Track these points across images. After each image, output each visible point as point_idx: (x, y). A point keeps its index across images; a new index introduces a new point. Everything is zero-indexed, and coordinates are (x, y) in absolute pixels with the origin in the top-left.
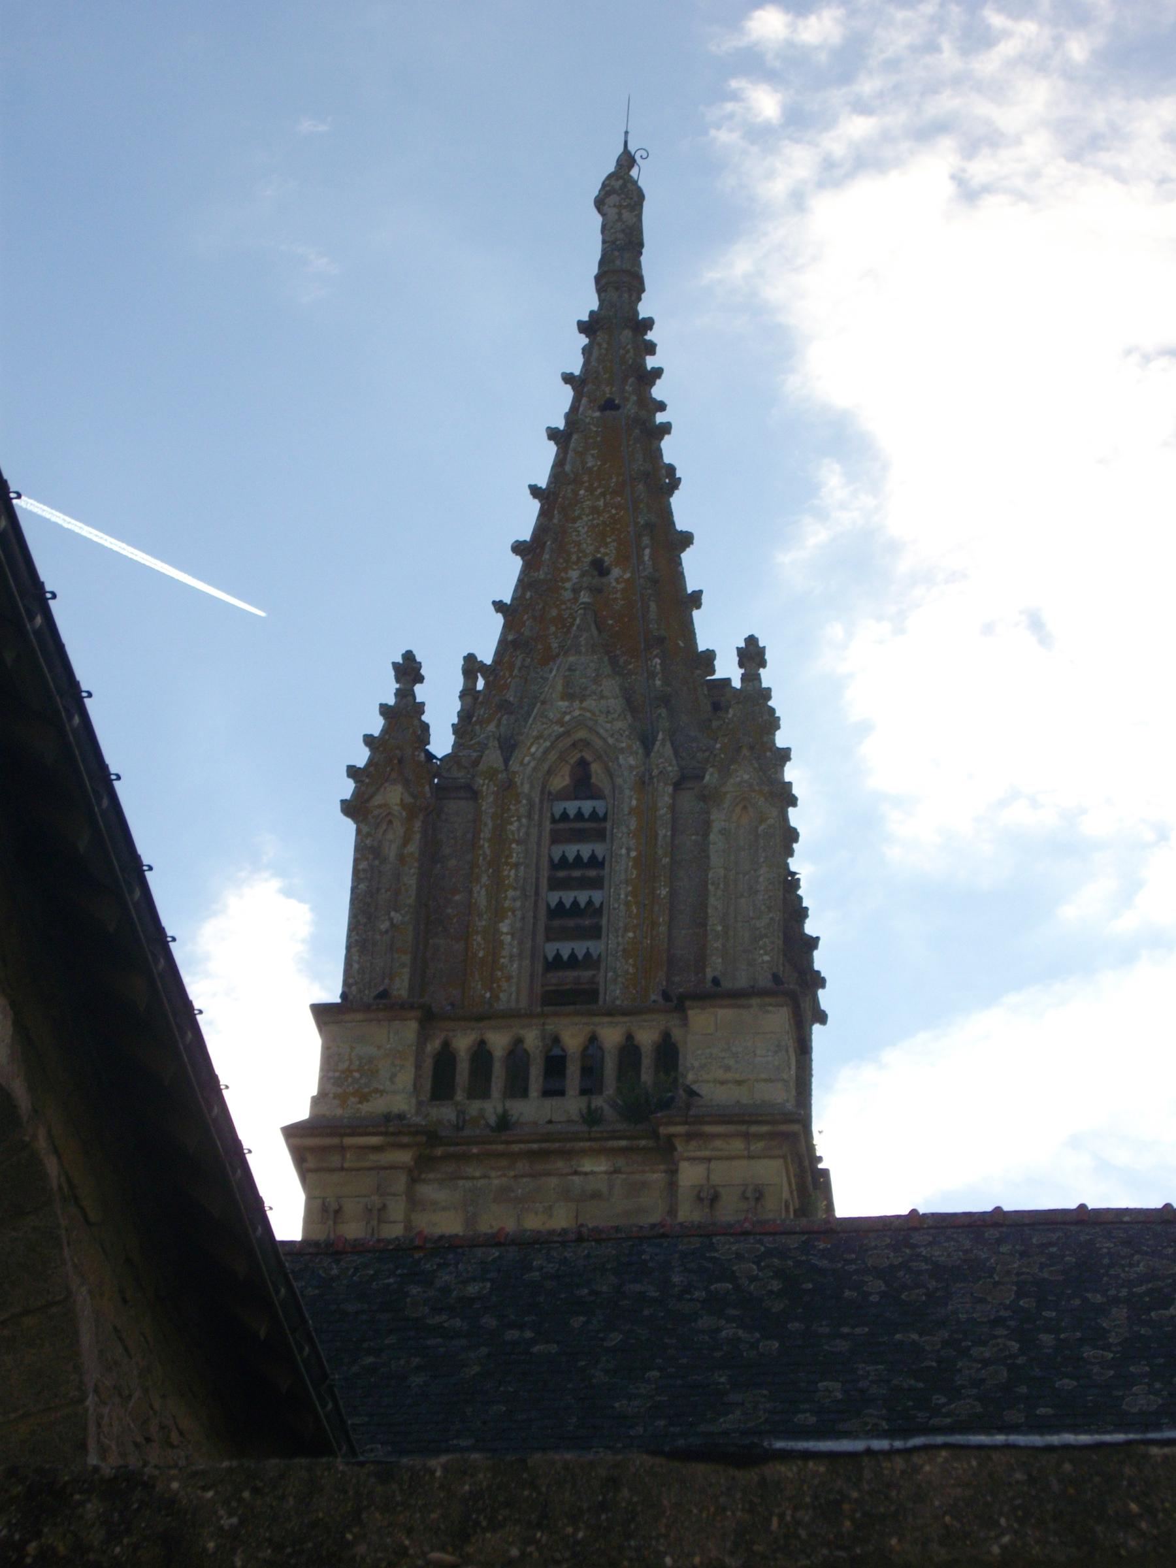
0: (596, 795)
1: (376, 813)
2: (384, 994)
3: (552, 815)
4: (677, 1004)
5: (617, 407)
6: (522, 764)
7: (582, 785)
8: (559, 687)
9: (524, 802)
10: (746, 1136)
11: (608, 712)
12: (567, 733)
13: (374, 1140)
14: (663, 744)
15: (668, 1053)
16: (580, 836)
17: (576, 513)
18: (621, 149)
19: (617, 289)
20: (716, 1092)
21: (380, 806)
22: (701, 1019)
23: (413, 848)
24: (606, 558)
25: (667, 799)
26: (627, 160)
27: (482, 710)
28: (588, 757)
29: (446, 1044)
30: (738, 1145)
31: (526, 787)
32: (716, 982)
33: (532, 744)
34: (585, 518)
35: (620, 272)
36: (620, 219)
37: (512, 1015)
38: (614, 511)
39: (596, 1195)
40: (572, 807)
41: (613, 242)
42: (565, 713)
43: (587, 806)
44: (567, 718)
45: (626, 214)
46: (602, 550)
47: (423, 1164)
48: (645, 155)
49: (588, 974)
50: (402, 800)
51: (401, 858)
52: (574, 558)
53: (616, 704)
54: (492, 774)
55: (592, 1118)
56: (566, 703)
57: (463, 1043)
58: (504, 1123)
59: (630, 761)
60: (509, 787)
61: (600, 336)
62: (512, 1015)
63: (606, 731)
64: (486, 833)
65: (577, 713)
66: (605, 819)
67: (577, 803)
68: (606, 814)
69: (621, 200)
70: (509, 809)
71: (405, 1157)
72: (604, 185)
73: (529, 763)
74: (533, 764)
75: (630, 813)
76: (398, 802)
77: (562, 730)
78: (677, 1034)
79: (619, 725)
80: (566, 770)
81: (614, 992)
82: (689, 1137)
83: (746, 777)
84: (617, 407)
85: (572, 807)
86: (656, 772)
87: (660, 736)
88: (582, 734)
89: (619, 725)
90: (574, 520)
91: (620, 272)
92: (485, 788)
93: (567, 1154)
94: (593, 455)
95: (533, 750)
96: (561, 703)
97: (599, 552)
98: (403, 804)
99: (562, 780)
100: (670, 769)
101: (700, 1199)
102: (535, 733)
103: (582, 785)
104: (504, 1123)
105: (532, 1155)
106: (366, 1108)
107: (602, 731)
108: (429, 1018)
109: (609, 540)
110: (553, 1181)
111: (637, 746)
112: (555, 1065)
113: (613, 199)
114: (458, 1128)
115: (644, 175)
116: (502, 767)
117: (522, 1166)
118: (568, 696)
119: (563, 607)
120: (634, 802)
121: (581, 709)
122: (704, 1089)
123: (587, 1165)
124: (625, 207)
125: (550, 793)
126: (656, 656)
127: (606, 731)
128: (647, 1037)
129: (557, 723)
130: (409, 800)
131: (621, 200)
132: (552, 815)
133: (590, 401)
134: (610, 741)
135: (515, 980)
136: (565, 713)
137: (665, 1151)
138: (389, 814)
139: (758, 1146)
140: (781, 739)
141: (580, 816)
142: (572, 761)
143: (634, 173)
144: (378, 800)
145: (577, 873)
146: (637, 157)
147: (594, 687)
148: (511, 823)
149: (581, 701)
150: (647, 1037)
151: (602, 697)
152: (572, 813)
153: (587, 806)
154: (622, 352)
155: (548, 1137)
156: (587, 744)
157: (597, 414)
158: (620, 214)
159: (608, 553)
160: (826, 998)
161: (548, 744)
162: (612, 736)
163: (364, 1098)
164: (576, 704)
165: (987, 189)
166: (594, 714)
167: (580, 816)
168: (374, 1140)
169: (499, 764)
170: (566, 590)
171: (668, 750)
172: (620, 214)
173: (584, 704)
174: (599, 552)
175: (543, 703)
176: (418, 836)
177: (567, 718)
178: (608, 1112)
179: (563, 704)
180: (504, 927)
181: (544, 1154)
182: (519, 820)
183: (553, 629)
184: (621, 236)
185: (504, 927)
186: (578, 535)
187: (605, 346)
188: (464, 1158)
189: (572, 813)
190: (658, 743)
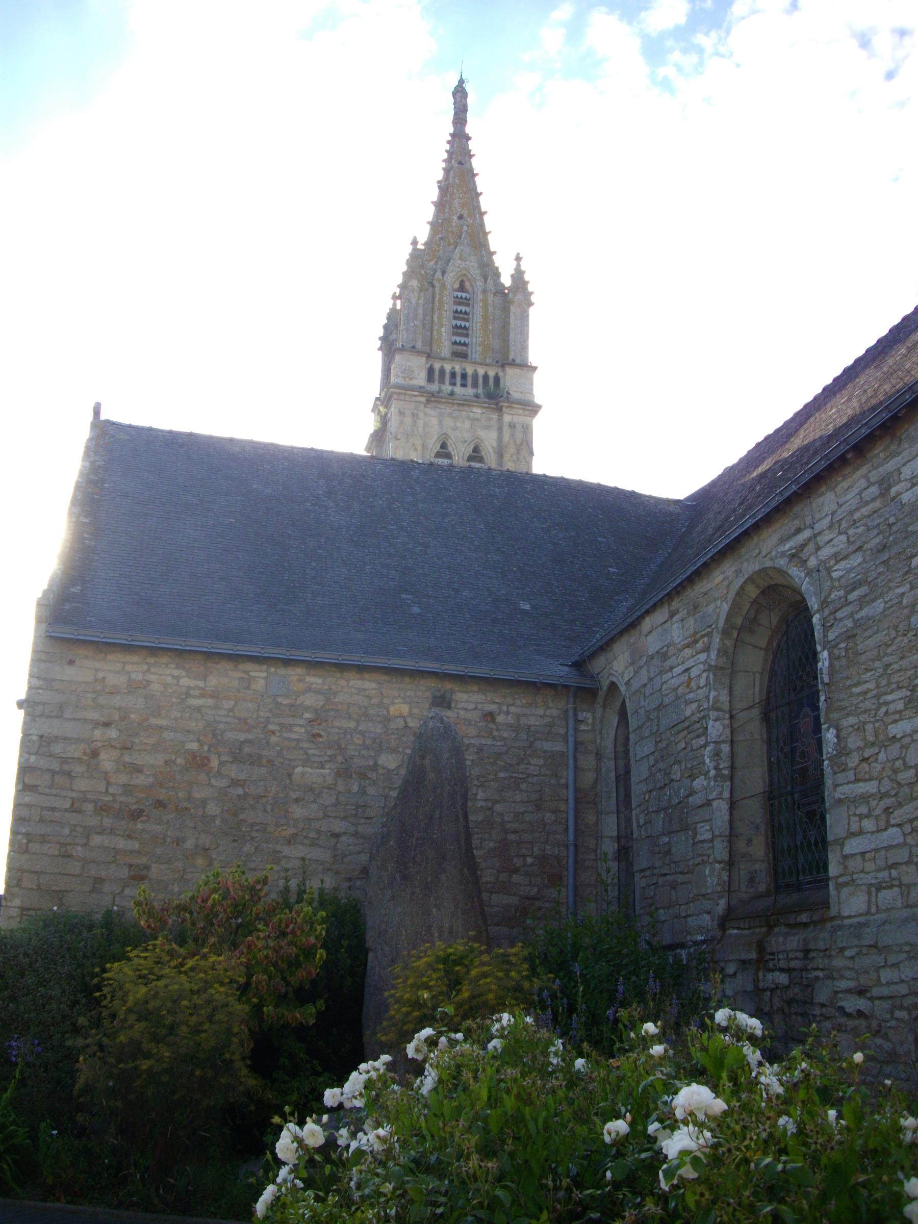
0: (467, 292)
2: (414, 347)
4: (503, 366)
7: (462, 288)
10: (524, 409)
13: (416, 393)
15: (497, 379)
16: (460, 304)
20: (515, 395)
22: (510, 371)
23: (421, 301)
26: (461, 82)
28: (465, 279)
29: (431, 366)
30: (521, 412)
32: (513, 360)
35: (460, 117)
37: (443, 359)
39: (477, 419)
43: (464, 295)
47: (428, 401)
49: (465, 348)
51: (418, 304)
53: (476, 265)
54: (439, 280)
55: (477, 396)
57: (437, 366)
58: (452, 394)
59: (480, 283)
60: (443, 286)
61: (457, 139)
62: (443, 359)
64: (437, 299)
69: (460, 93)
71: (423, 399)
78: (501, 374)
80: (458, 283)
81: (477, 357)
82: (507, 407)
85: (459, 294)
88: (464, 272)
91: (460, 117)
93: (469, 406)
99: (457, 286)
101: (510, 426)
103: (462, 288)
104: (452, 394)
105: (459, 405)
106: (411, 382)
108: (429, 356)
110: (464, 413)
112: (453, 375)
114: (438, 392)
115: (468, 87)
117: (455, 407)
118: (461, 259)
122: (511, 393)
123: (475, 410)
128: (491, 374)
131: (460, 93)
135: (446, 349)
137: (499, 410)
139: (527, 413)
141: (461, 297)
144: (410, 284)
145: (461, 316)
150: (491, 374)
153: (464, 295)
155: (466, 400)
159: (465, 213)
160: (379, 343)
163: (411, 379)
167: (461, 297)
168: (416, 393)
169: (441, 277)
171: (492, 282)
178: (482, 395)
179: (459, 262)
180: (443, 330)
181: (463, 405)
185: (443, 330)
188: (439, 402)
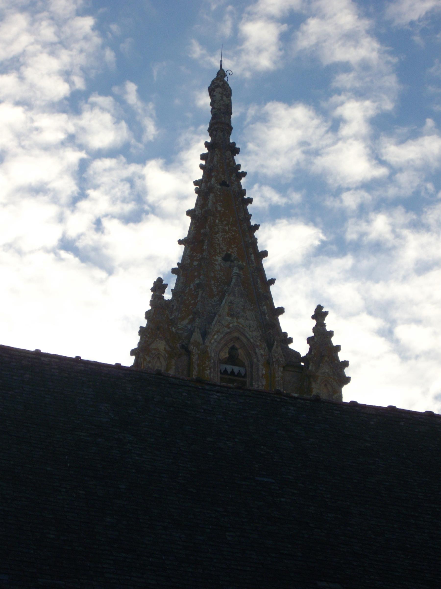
1: (153, 352)
3: (220, 371)
5: (228, 186)
6: (210, 342)
8: (226, 310)
9: (212, 361)
11: (250, 327)
12: (230, 333)
14: (277, 347)
17: (216, 230)
18: (219, 69)
19: (222, 131)
21: (155, 349)
24: (233, 254)
25: (280, 373)
27: (177, 314)
28: (237, 346)
31: (213, 354)
33: (214, 335)
34: (220, 234)
36: (222, 99)
38: (233, 233)
40: (229, 368)
41: (220, 109)
42: (230, 323)
43: (236, 369)
44: (231, 325)
45: (225, 98)
46: (231, 250)
48: (231, 73)
50: (165, 348)
52: (218, 251)
56: (230, 318)
61: (217, 151)
63: (249, 335)
65: (235, 324)
66: (245, 376)
67: (232, 367)
68: (245, 374)
70: (205, 363)
72: (213, 82)
73: (214, 343)
74: (215, 344)
75: (262, 376)
76: (164, 349)
77: (229, 330)
79: (255, 334)
80: (227, 350)
83: (327, 371)
84: (228, 186)
85: (229, 368)
86: (274, 360)
87: (275, 343)
88: (236, 334)
89: (255, 334)
90: (216, 233)
92: (194, 350)
94: (220, 205)
95: (215, 337)
96: (227, 318)
97: (229, 251)
98: (165, 349)
99: (225, 355)
100: (281, 359)
102: (216, 329)
107: (247, 335)
109: (233, 246)
111: (264, 345)
113: (218, 90)
116: (202, 342)
119: (216, 273)
120: (264, 372)
121: (237, 322)
124: (225, 95)
125: (220, 360)
126: (264, 305)
127: (249, 335)
129: (226, 327)
130: (168, 348)
132: (220, 371)
133: (216, 180)
134: (252, 340)
136: (230, 323)
138: (159, 354)
140: (342, 356)
141: (232, 373)
142: (230, 346)
143: (226, 79)
144: (153, 346)
146: (227, 74)
147: (243, 313)
148: (207, 370)
149: (237, 319)
151: (247, 319)
152: (229, 371)
154: (227, 161)
156: (238, 339)
157: (219, 187)
158: (222, 97)
161: (222, 336)
162: (252, 338)
164: (235, 319)
165: (63, 144)
166: (243, 326)
167: (232, 373)
170: (216, 265)
172: (222, 97)
173: (239, 321)
174: (229, 251)
175: (220, 316)
176: (174, 368)
177: (231, 325)
182: (210, 369)
183: (213, 282)
184: (223, 107)
186: (218, 241)
187: (219, 156)
189: (229, 371)
190: (275, 346)
